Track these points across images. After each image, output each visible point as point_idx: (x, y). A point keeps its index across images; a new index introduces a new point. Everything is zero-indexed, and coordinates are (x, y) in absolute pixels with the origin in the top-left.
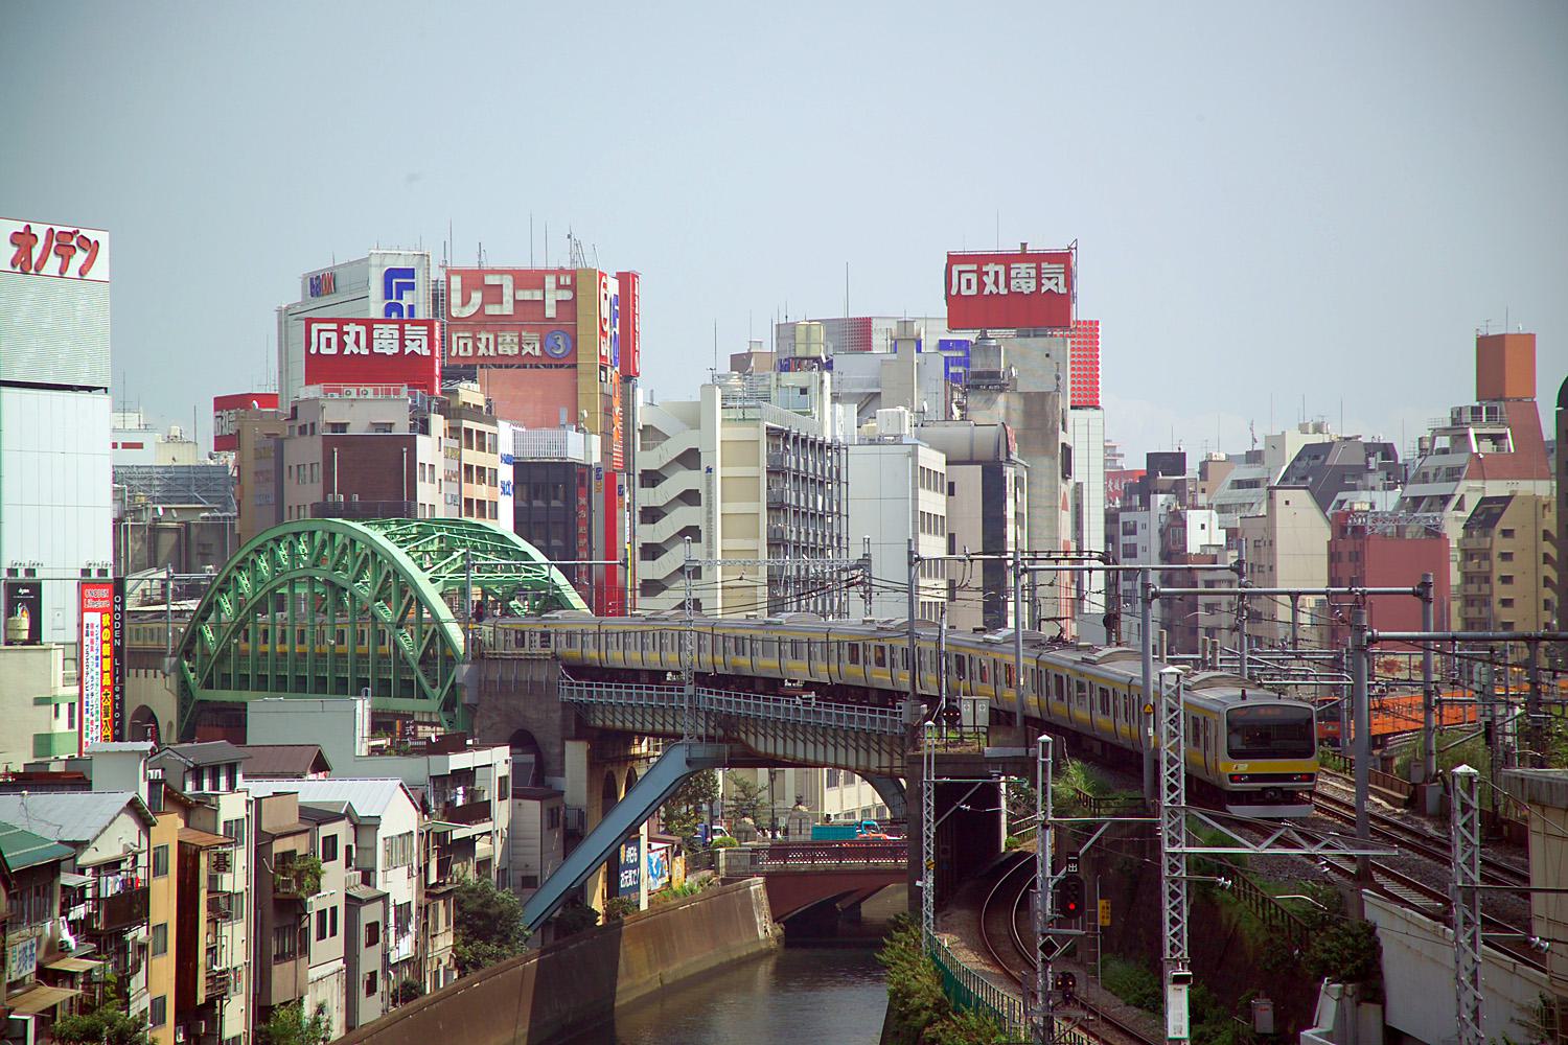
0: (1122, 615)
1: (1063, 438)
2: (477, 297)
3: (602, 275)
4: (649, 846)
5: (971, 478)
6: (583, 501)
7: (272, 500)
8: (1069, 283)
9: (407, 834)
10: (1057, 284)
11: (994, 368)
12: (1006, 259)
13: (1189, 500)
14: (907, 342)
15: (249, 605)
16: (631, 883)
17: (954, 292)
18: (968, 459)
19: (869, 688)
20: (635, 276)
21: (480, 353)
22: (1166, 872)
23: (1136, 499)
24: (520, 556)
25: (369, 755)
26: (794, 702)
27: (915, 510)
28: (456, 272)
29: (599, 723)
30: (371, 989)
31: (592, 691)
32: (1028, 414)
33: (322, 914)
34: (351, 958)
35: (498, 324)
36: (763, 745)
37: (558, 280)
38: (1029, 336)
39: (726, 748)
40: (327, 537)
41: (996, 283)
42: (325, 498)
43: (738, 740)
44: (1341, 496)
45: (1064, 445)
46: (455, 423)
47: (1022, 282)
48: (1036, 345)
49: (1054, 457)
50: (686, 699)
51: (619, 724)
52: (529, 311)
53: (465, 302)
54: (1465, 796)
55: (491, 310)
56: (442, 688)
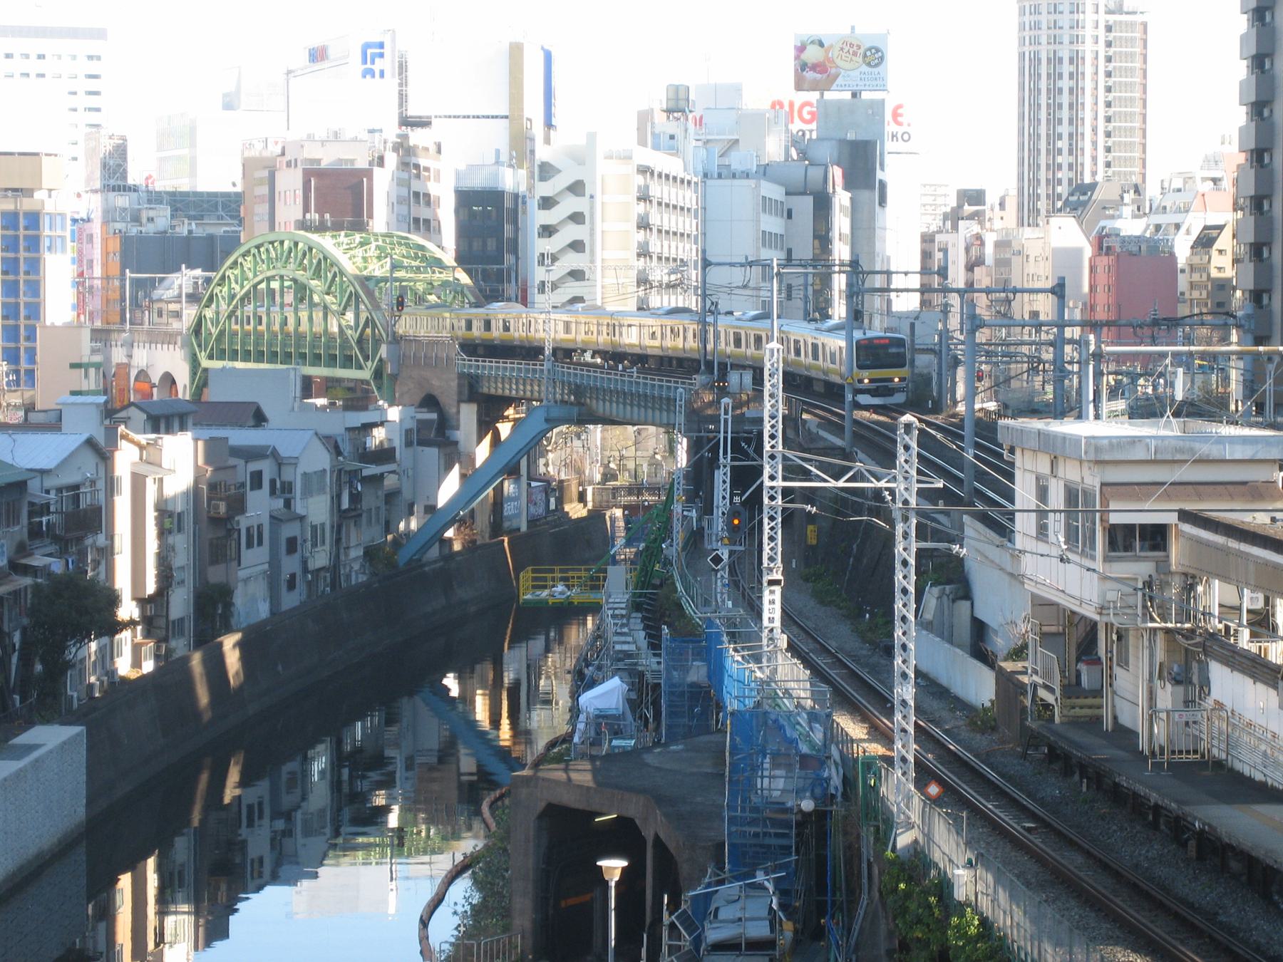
4: (529, 485)
15: (238, 297)
18: (802, 190)
22: (766, 500)
23: (949, 224)
29: (485, 390)
30: (291, 584)
34: (274, 563)
36: (600, 408)
42: (304, 216)
44: (1102, 223)
45: (881, 181)
50: (546, 372)
51: (500, 392)
56: (373, 361)
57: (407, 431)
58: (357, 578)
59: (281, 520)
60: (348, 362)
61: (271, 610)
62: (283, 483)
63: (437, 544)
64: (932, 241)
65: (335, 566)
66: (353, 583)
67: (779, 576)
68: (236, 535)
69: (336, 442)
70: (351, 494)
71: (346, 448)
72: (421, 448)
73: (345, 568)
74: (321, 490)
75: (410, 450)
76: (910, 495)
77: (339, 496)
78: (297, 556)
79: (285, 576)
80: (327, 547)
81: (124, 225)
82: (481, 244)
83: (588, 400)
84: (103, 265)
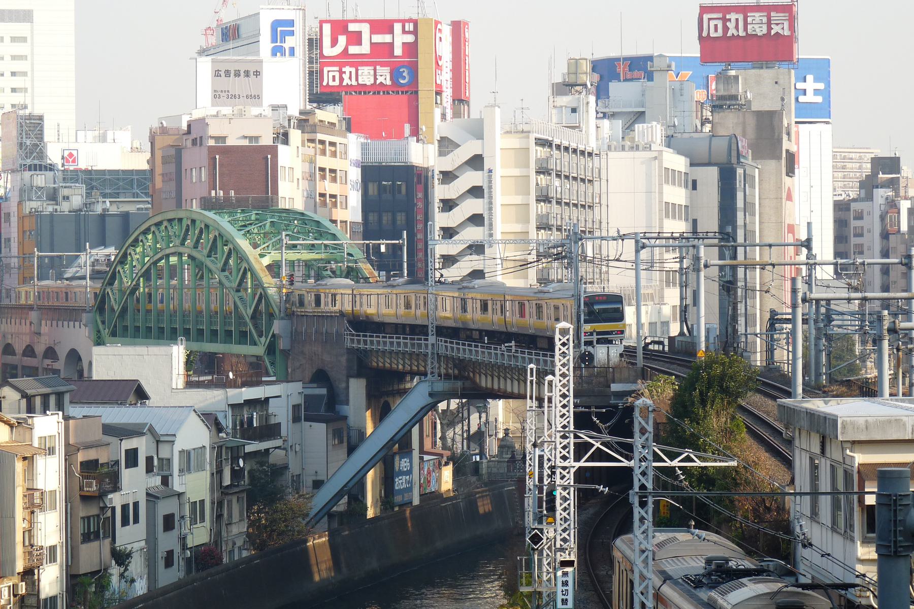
0: (29, 302)
1: (786, 145)
2: (342, 40)
3: (437, 23)
4: (421, 458)
5: (710, 177)
6: (420, 195)
7: (173, 195)
8: (792, 28)
9: (201, 448)
10: (783, 28)
11: (733, 92)
12: (744, 10)
13: (902, 193)
14: (661, 72)
16: (404, 486)
17: (705, 34)
18: (707, 161)
19: (537, 336)
20: (466, 24)
21: (344, 84)
24: (329, 236)
25: (184, 388)
26: (501, 348)
27: (661, 202)
28: (326, 22)
30: (169, 560)
31: (367, 340)
32: (759, 127)
33: (125, 508)
34: (151, 539)
35: (358, 61)
36: (484, 382)
37: (404, 27)
38: (762, 68)
39: (459, 384)
40: (189, 223)
41: (737, 27)
43: (468, 378)
45: (787, 151)
46: (311, 136)
47: (756, 26)
48: (767, 74)
49: (779, 158)
50: (430, 347)
52: (382, 52)
53: (334, 42)
54: (643, 423)
55: (353, 50)
56: (266, 338)
57: (294, 406)
58: (240, 553)
59: (157, 498)
60: (244, 338)
61: (149, 587)
62: (161, 460)
63: (326, 518)
64: (848, 209)
65: (216, 542)
66: (236, 558)
67: (573, 557)
68: (109, 514)
69: (216, 419)
70: (233, 471)
71: (227, 422)
72: (309, 423)
73: (227, 544)
74: (201, 468)
75: (298, 425)
76: (647, 480)
77: (220, 472)
78: (175, 533)
79: (161, 553)
80: (207, 523)
81: (39, 203)
82: (390, 218)
83: (471, 375)
84: (19, 243)
